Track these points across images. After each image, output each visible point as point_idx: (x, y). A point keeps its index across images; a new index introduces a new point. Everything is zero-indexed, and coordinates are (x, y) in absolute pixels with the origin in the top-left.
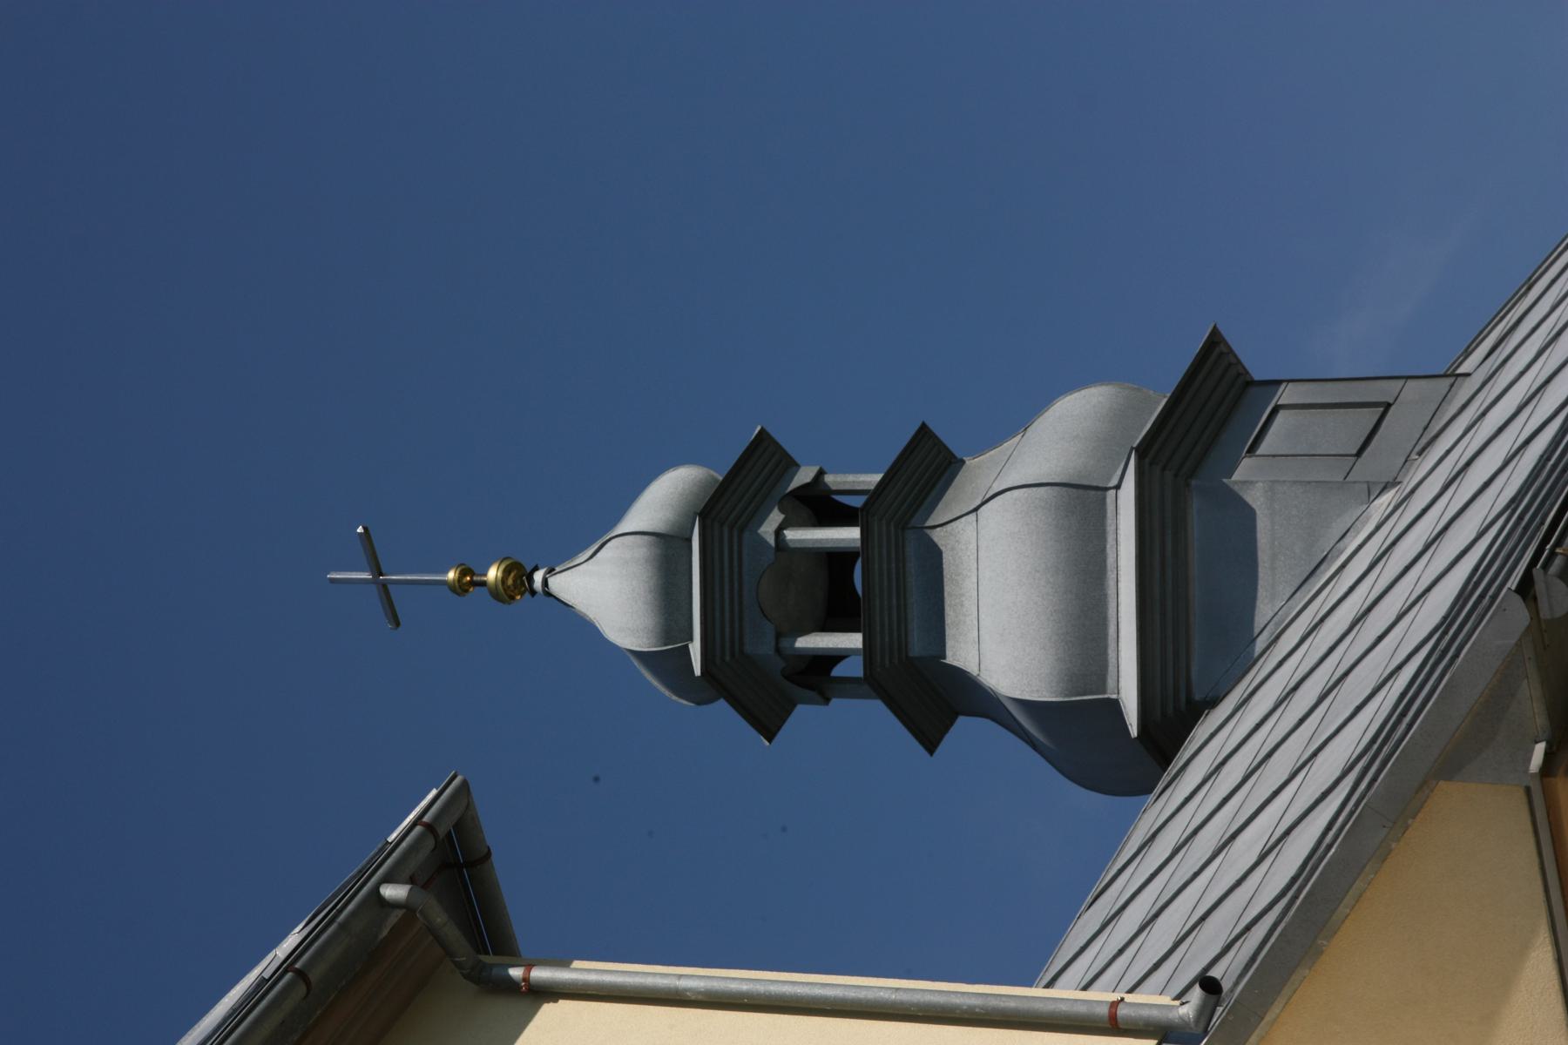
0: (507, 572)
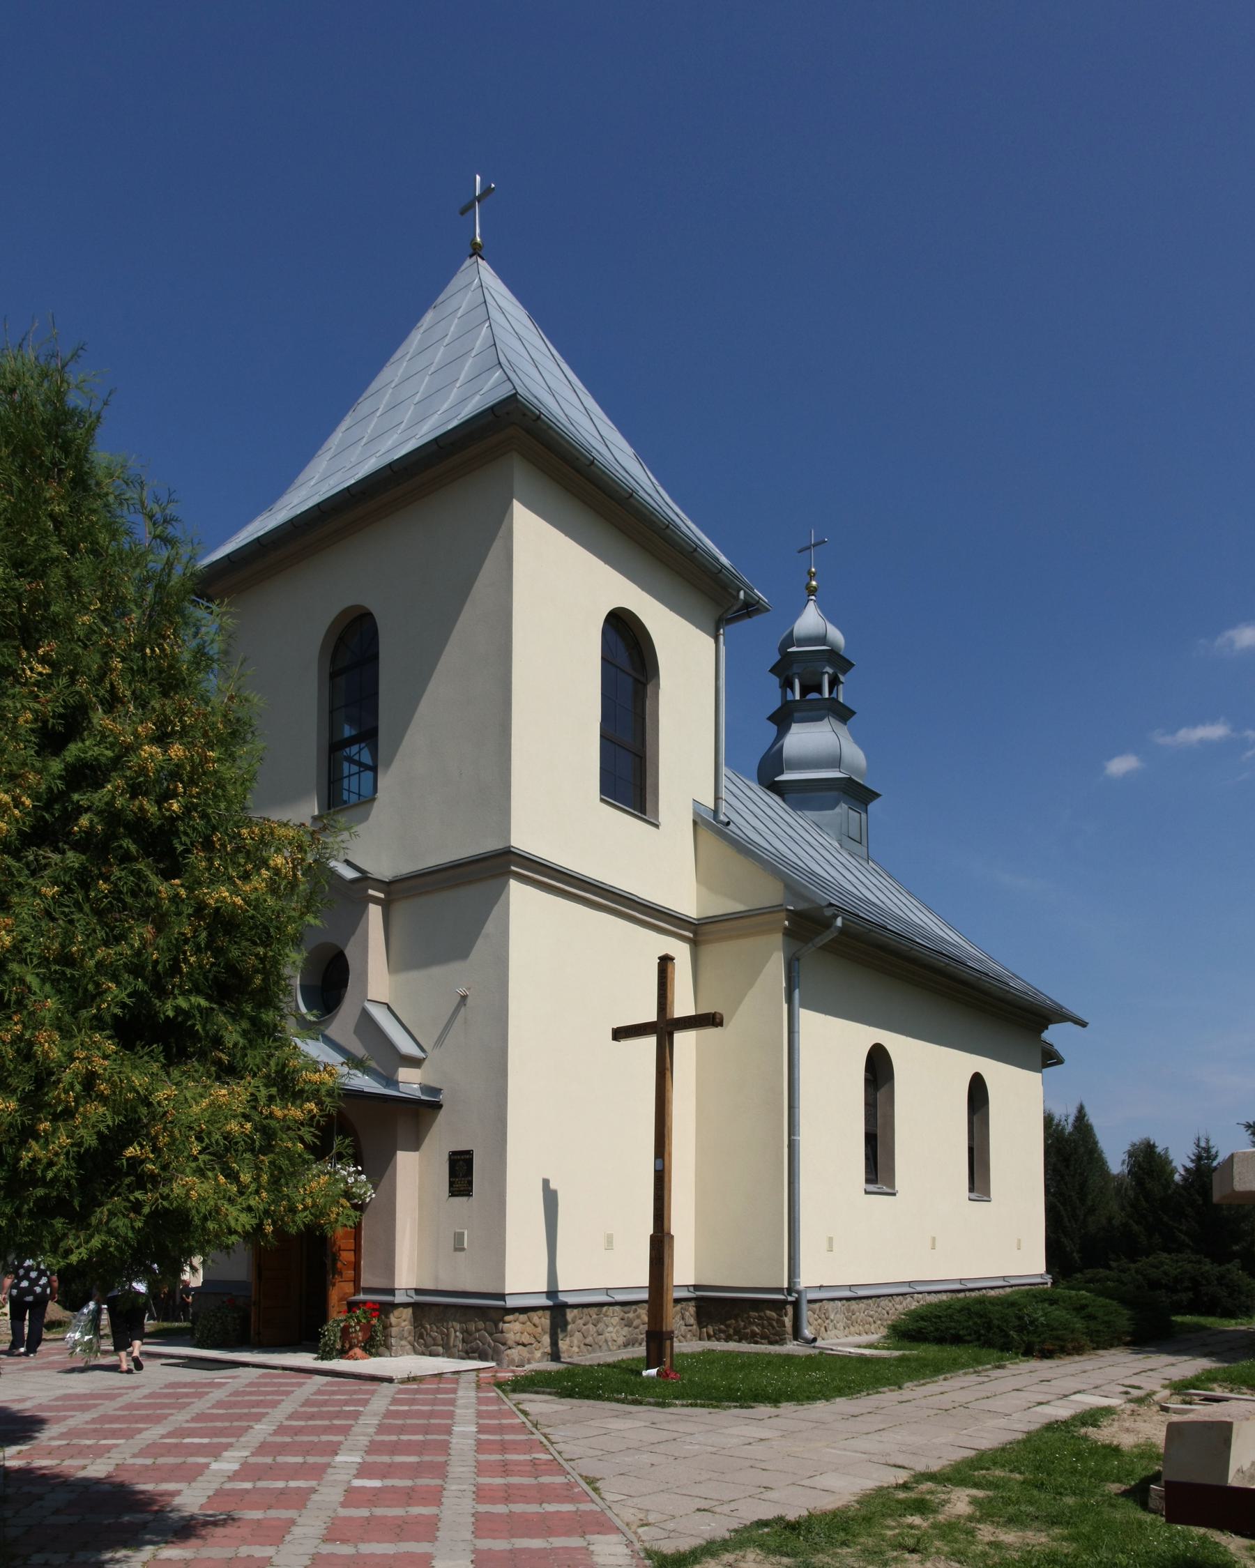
0: (815, 587)
